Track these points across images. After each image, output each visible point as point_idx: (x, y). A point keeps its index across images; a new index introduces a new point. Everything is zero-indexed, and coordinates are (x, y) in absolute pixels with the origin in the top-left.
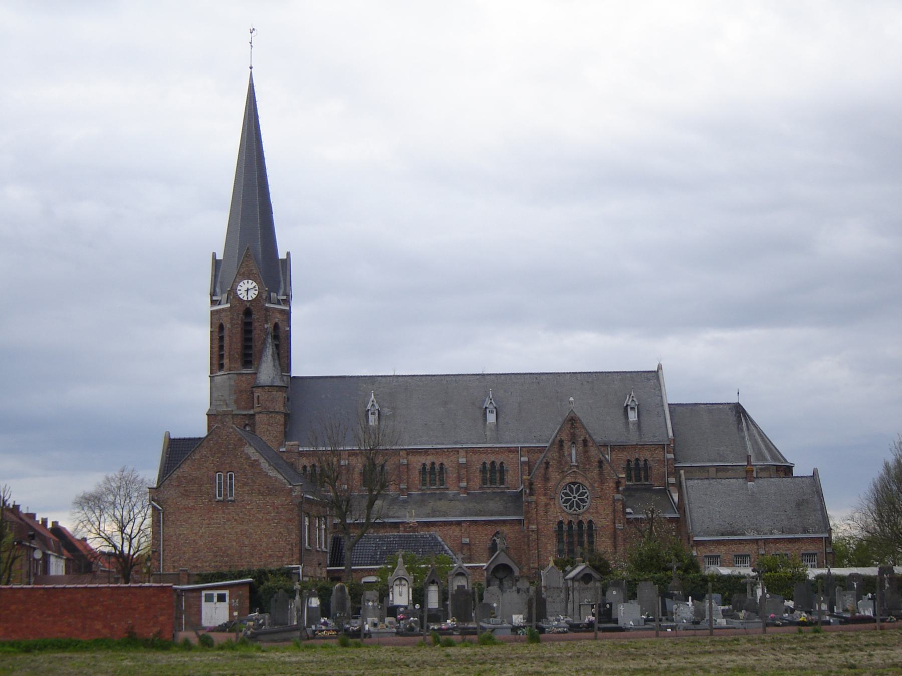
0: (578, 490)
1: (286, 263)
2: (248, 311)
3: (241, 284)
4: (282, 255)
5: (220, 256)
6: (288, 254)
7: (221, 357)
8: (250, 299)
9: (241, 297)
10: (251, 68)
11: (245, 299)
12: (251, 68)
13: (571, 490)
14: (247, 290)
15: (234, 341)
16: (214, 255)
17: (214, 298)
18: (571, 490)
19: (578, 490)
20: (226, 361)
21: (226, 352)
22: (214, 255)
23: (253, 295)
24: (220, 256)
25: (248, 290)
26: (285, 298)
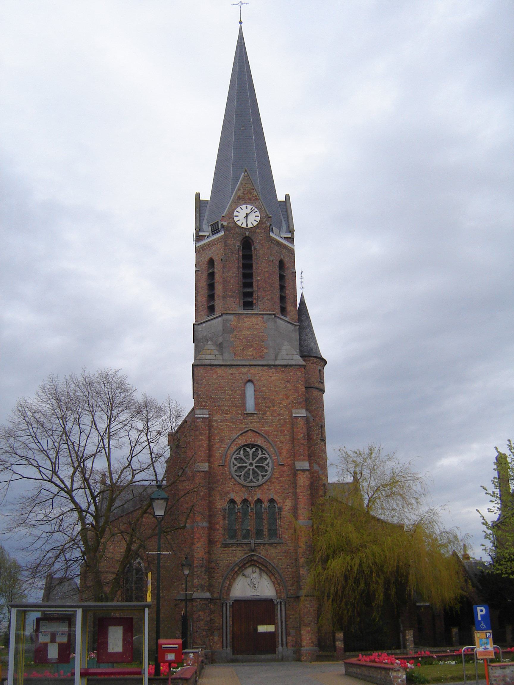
0: (255, 455)
1: (286, 205)
2: (247, 242)
3: (238, 209)
4: (281, 197)
5: (206, 196)
6: (287, 197)
7: (211, 297)
8: (250, 226)
9: (239, 223)
10: (241, 23)
11: (244, 226)
12: (241, 23)
13: (247, 455)
14: (246, 216)
15: (229, 276)
16: (198, 195)
17: (201, 234)
18: (247, 455)
19: (255, 455)
20: (218, 303)
21: (219, 288)
22: (198, 195)
23: (254, 220)
24: (206, 196)
25: (246, 217)
26: (289, 235)
